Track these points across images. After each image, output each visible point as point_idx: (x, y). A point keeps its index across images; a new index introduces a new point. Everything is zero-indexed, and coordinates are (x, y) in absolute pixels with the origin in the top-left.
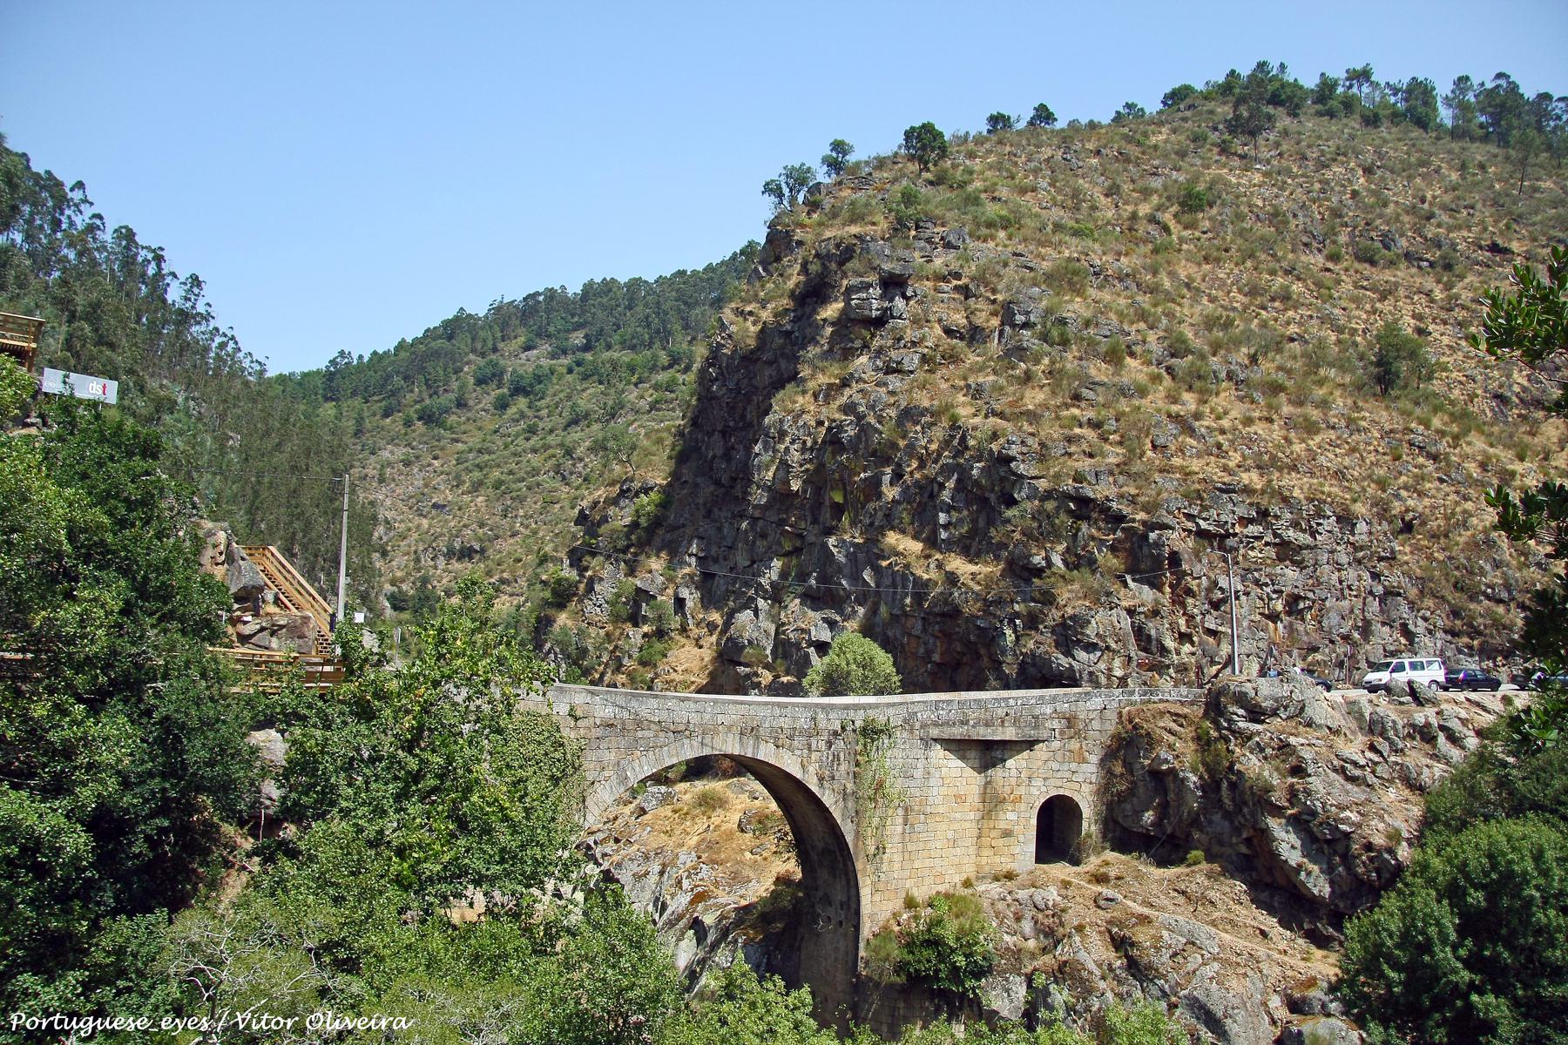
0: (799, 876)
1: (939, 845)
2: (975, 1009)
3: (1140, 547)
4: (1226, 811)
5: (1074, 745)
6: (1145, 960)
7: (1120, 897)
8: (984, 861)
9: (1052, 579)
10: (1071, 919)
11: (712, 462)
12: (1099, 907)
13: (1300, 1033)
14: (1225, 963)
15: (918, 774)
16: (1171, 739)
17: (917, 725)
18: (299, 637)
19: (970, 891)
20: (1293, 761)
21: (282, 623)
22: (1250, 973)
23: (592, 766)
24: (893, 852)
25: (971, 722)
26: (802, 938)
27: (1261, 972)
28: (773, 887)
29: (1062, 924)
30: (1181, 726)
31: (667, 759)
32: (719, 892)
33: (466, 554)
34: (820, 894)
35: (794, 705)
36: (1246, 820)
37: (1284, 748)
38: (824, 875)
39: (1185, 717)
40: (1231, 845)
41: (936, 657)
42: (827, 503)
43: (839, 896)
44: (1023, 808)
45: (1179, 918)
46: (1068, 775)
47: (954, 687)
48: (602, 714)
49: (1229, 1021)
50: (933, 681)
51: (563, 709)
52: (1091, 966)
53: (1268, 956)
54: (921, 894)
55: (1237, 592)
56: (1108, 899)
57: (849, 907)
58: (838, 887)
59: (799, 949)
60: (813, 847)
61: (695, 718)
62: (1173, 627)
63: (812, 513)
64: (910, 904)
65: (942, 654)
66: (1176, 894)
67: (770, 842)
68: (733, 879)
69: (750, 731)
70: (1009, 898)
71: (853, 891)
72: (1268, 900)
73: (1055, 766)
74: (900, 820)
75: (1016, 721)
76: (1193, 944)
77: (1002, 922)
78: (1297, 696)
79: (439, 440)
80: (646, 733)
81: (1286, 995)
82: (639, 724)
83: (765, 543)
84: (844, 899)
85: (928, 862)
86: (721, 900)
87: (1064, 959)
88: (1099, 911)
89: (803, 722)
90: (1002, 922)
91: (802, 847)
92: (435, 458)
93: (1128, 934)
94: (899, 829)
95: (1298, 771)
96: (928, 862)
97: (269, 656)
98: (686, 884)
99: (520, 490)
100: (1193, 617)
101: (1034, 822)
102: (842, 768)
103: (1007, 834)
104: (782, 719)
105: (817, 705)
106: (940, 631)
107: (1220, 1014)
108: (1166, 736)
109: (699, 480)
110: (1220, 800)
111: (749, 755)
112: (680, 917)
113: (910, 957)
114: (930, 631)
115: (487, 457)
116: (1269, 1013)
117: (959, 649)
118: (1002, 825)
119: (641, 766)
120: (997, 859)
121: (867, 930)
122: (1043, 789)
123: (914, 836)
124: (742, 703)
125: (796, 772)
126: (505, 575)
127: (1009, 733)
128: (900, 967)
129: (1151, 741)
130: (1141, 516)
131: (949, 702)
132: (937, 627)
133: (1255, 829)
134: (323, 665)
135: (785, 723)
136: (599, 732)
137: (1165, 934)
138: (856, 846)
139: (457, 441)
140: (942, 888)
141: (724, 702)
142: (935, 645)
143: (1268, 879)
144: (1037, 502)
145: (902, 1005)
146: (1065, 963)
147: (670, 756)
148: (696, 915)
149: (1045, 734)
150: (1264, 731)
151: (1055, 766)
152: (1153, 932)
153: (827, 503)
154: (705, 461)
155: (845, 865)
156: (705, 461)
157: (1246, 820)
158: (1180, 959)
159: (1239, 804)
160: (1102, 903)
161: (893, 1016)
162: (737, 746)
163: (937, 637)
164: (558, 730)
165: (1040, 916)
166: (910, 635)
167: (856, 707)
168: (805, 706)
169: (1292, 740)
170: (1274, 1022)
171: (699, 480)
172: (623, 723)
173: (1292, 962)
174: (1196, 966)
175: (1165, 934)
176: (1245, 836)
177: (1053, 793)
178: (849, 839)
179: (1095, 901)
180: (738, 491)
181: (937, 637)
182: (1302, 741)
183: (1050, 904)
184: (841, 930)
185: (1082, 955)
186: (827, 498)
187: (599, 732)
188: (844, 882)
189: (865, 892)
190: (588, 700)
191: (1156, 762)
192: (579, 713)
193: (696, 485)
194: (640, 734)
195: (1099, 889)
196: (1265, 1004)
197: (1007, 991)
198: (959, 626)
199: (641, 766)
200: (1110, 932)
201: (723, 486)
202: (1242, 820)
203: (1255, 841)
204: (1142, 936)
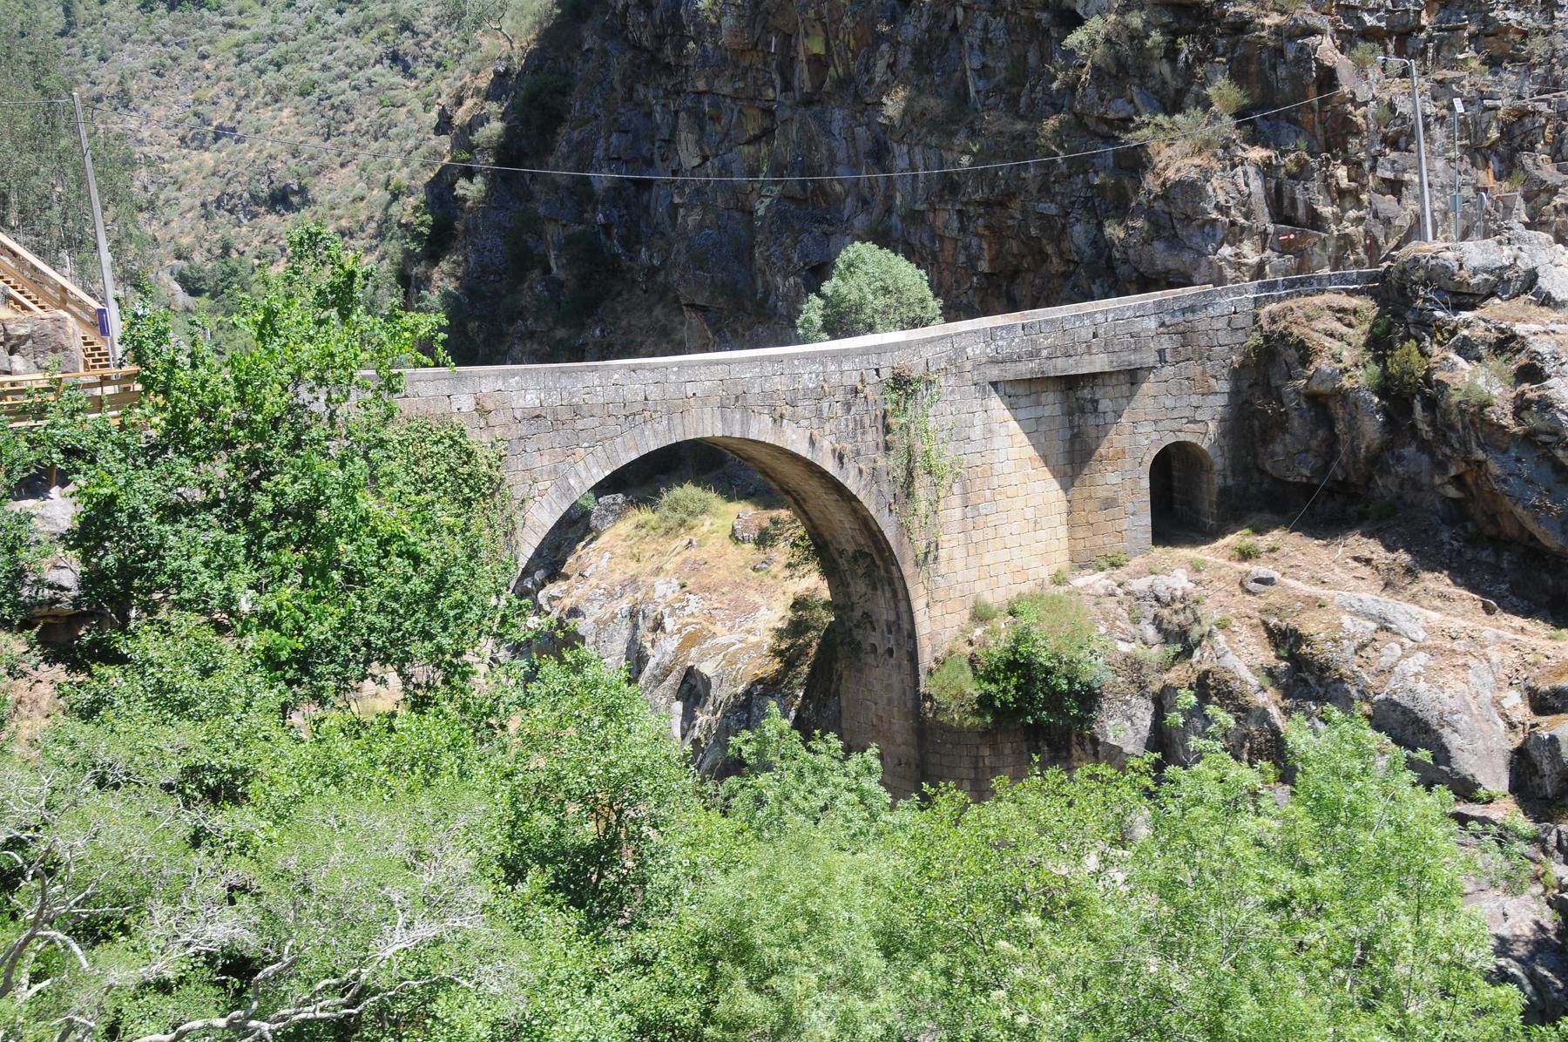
0: (826, 594)
1: (1015, 528)
2: (1088, 747)
3: (1274, 67)
4: (1423, 440)
5: (1194, 369)
6: (1320, 658)
7: (1277, 576)
8: (1080, 546)
9: (1145, 131)
10: (1211, 613)
11: (624, 15)
12: (1248, 592)
13: (1553, 740)
14: (1433, 651)
15: (977, 433)
16: (1336, 346)
17: (968, 366)
18: (54, 350)
19: (1062, 589)
20: (1522, 359)
21: (22, 331)
22: (1472, 662)
23: (519, 478)
24: (951, 547)
25: (1044, 353)
26: (840, 678)
27: (1488, 661)
28: (790, 614)
29: (1197, 620)
30: (1350, 325)
31: (622, 455)
32: (718, 628)
33: (281, 200)
34: (857, 614)
35: (792, 357)
36: (1454, 450)
37: (1506, 343)
38: (859, 587)
39: (1355, 312)
40: (1433, 488)
41: (984, 266)
42: (802, 57)
43: (884, 614)
44: (1127, 466)
45: (1364, 596)
46: (1188, 413)
47: (1013, 306)
48: (521, 403)
49: (1446, 732)
50: (982, 301)
51: (465, 402)
52: (1245, 673)
53: (1499, 637)
54: (995, 597)
55: (1425, 116)
56: (1259, 581)
57: (899, 628)
58: (882, 602)
59: (837, 693)
60: (841, 553)
61: (654, 393)
62: (1328, 183)
63: (782, 74)
64: (980, 615)
65: (991, 261)
66: (1356, 564)
67: (781, 552)
68: (736, 608)
69: (738, 400)
70: (1119, 591)
71: (898, 585)
72: (1492, 560)
73: (1170, 402)
74: (956, 501)
75: (1107, 348)
76: (1388, 629)
77: (1113, 626)
78: (1524, 264)
79: (202, 28)
80: (588, 422)
81: (1529, 688)
82: (576, 411)
83: (718, 128)
84: (892, 617)
85: (1004, 555)
86: (721, 640)
87: (1205, 667)
88: (1248, 597)
89: (808, 380)
90: (1113, 626)
91: (821, 549)
92: (204, 57)
93: (1293, 625)
94: (958, 513)
95: (1532, 373)
96: (1004, 555)
97: (13, 384)
98: (669, 623)
99: (344, 92)
100: (1359, 164)
101: (1145, 483)
102: (869, 437)
103: (1109, 503)
104: (777, 379)
105: (823, 353)
106: (986, 227)
107: (1434, 723)
108: (1327, 342)
109: (608, 45)
110: (1413, 427)
111: (737, 435)
112: (666, 672)
113: (993, 688)
114: (971, 228)
115: (282, 46)
116: (1504, 716)
117: (1015, 250)
118: (1101, 492)
119: (588, 469)
120: (1099, 541)
121: (926, 659)
122: (1155, 436)
123: (980, 520)
124: (718, 363)
125: (802, 449)
126: (344, 223)
127: (1098, 363)
128: (985, 701)
129: (1305, 354)
130: (1273, 19)
131: (1009, 328)
132: (981, 221)
133: (1467, 463)
134: (101, 385)
135: (780, 384)
136: (523, 429)
137: (1346, 620)
138: (900, 544)
139: (230, 26)
140: (1024, 589)
141: (691, 365)
142: (980, 248)
143: (1491, 530)
144: (1112, 17)
145: (986, 752)
146: (1206, 674)
147: (627, 451)
148: (690, 664)
149: (1151, 359)
150: (1475, 323)
151: (1170, 402)
152: (1326, 618)
153: (802, 57)
154: (614, 14)
155: (888, 571)
156: (614, 14)
157: (1454, 450)
158: (1368, 652)
159: (1443, 429)
160: (1252, 586)
161: (976, 768)
162: (719, 424)
163: (982, 236)
164: (463, 435)
165: (1166, 612)
166: (942, 238)
167: (880, 350)
168: (809, 358)
169: (1519, 329)
170: (1512, 726)
171: (608, 45)
172: (554, 412)
173: (1534, 642)
174: (1393, 660)
175: (1346, 620)
176: (1453, 472)
177: (1170, 439)
178: (890, 534)
179: (1241, 584)
180: (668, 52)
181: (982, 236)
182: (1534, 327)
183: (1179, 593)
184: (892, 661)
185: (1230, 660)
186: (801, 49)
187: (523, 429)
188: (888, 595)
189: (919, 605)
190: (500, 385)
191: (1315, 381)
192: (489, 405)
193: (605, 52)
194: (580, 424)
195: (1246, 566)
196: (1497, 703)
197: (1129, 718)
198: (1012, 218)
199: (588, 469)
200: (1265, 623)
201: (646, 50)
202: (1448, 451)
203: (1469, 480)
204: (1310, 625)
